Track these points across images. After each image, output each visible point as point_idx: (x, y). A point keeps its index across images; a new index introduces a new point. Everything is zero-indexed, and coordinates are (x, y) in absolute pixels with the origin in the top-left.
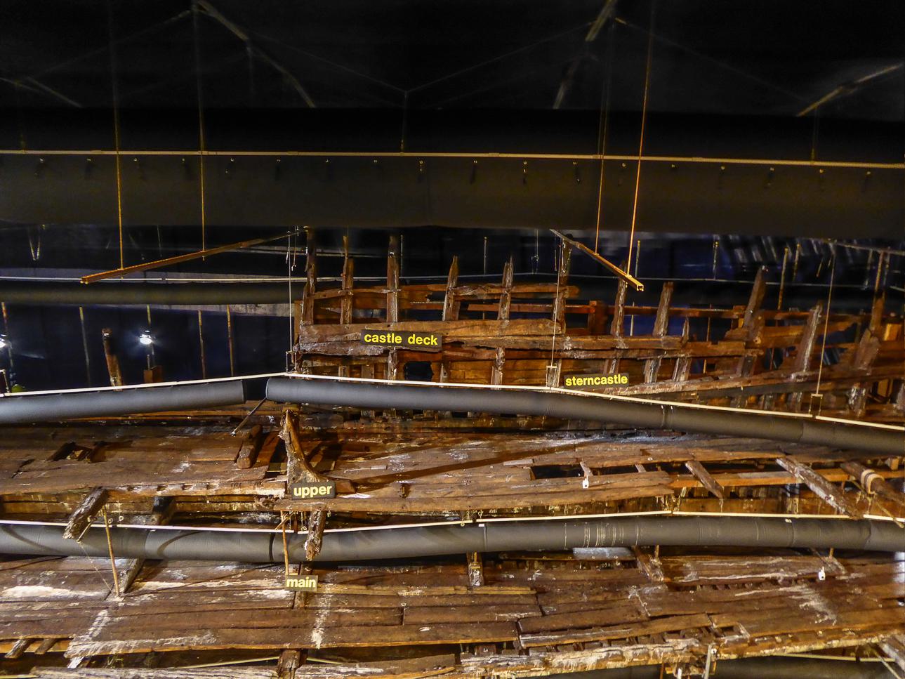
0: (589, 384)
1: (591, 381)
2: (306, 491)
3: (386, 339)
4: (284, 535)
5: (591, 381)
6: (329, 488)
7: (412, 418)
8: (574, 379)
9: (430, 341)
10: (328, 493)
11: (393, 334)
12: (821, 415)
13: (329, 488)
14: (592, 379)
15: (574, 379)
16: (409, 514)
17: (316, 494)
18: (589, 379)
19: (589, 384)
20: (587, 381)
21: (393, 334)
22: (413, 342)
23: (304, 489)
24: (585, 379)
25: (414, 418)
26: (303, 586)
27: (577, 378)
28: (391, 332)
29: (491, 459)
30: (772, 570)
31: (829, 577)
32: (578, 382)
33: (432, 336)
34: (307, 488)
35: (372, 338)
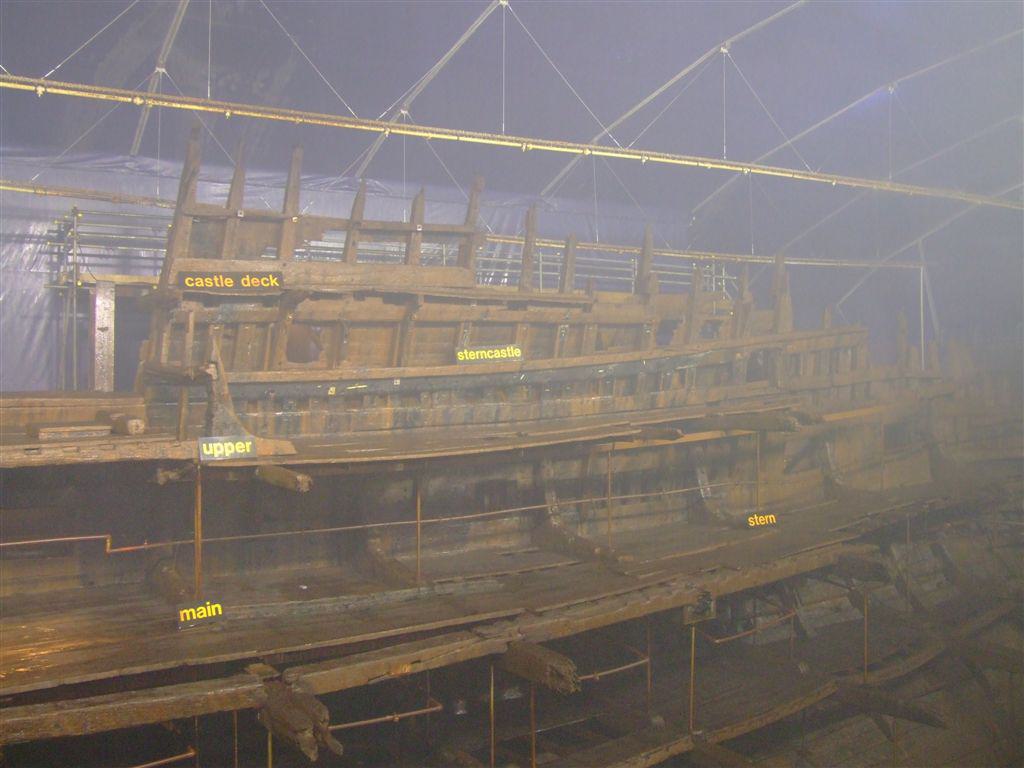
0: (188, 618)
1: (191, 614)
2: (219, 449)
3: (213, 281)
5: (191, 614)
7: (402, 379)
8: (466, 352)
9: (269, 282)
10: (248, 451)
11: (221, 277)
12: (474, 347)
14: (193, 610)
15: (466, 352)
17: (232, 451)
18: (482, 352)
19: (188, 618)
21: (221, 277)
23: (216, 445)
24: (477, 353)
25: (398, 382)
26: (205, 615)
27: (468, 351)
31: (361, 177)
33: (271, 276)
35: (194, 282)
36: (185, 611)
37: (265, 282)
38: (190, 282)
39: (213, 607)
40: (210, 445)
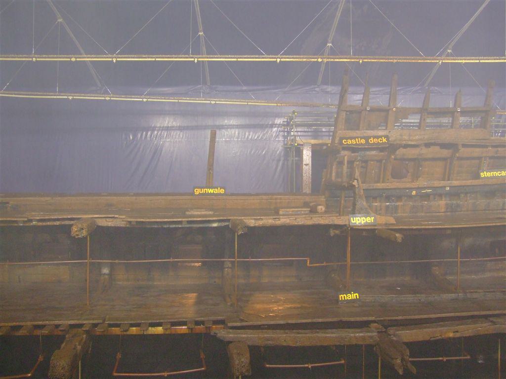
0: (343, 299)
1: (344, 297)
2: (358, 220)
3: (356, 141)
4: (236, 262)
5: (344, 297)
6: (373, 218)
9: (382, 140)
10: (372, 221)
13: (373, 218)
15: (485, 173)
16: (500, 58)
18: (494, 173)
19: (343, 299)
20: (493, 174)
22: (372, 142)
23: (357, 218)
26: (351, 298)
28: (358, 138)
29: (281, 329)
30: (449, 232)
32: (488, 174)
34: (359, 218)
35: (347, 142)
36: (342, 295)
37: (381, 140)
38: (345, 142)
39: (355, 295)
40: (355, 218)
